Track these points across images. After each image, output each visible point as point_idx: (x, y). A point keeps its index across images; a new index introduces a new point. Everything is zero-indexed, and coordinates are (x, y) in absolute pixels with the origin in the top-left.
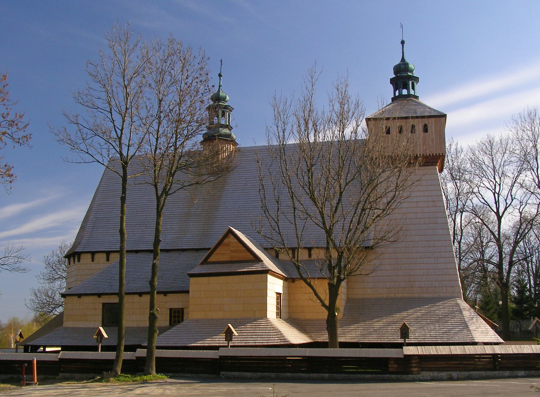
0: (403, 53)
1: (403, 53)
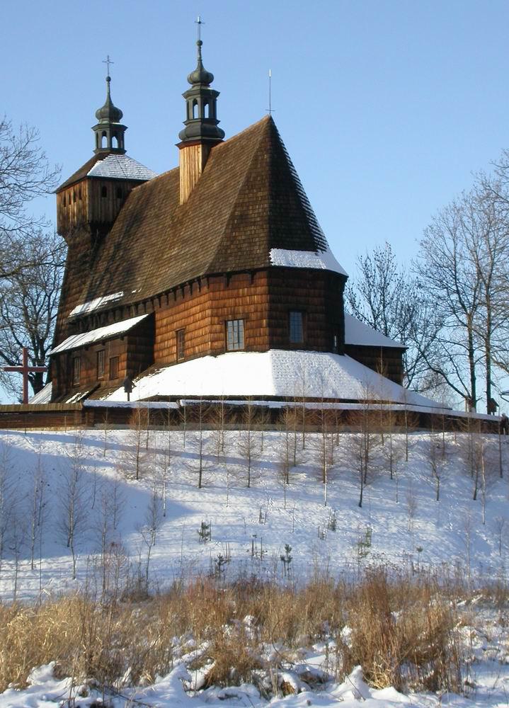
0: (109, 93)
1: (109, 93)
